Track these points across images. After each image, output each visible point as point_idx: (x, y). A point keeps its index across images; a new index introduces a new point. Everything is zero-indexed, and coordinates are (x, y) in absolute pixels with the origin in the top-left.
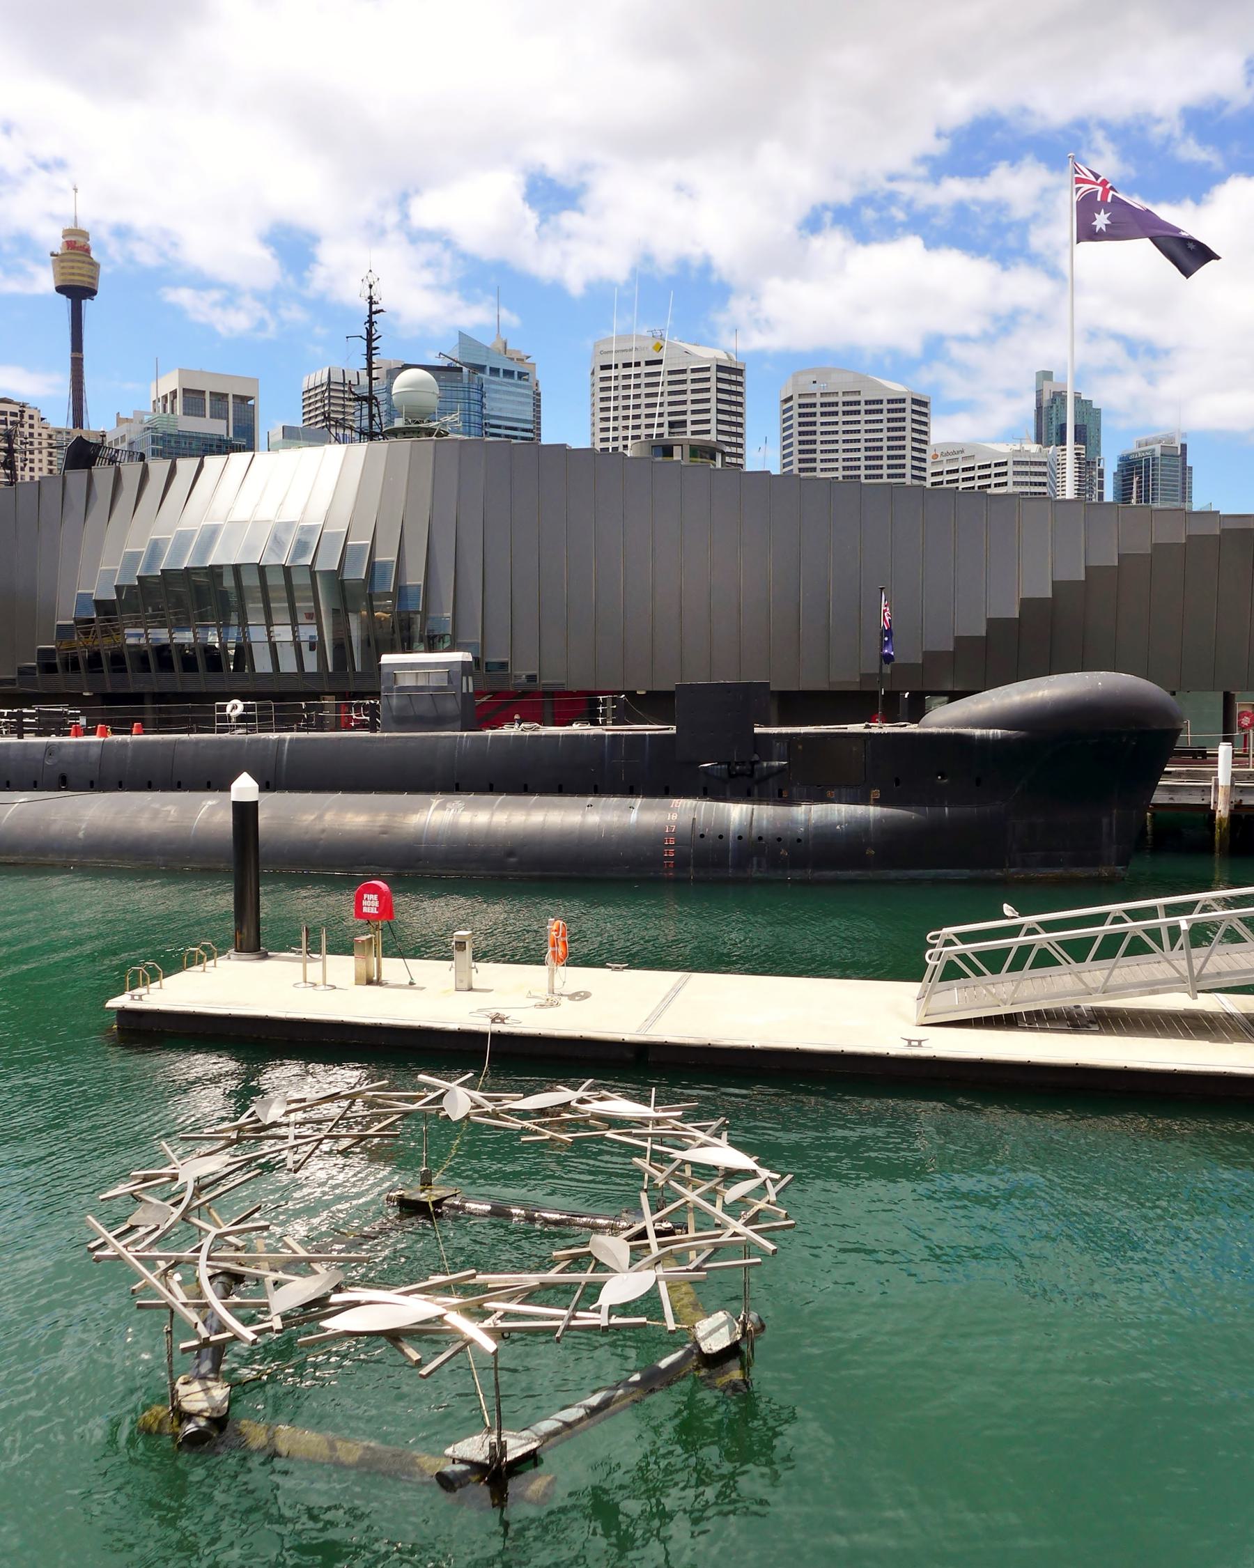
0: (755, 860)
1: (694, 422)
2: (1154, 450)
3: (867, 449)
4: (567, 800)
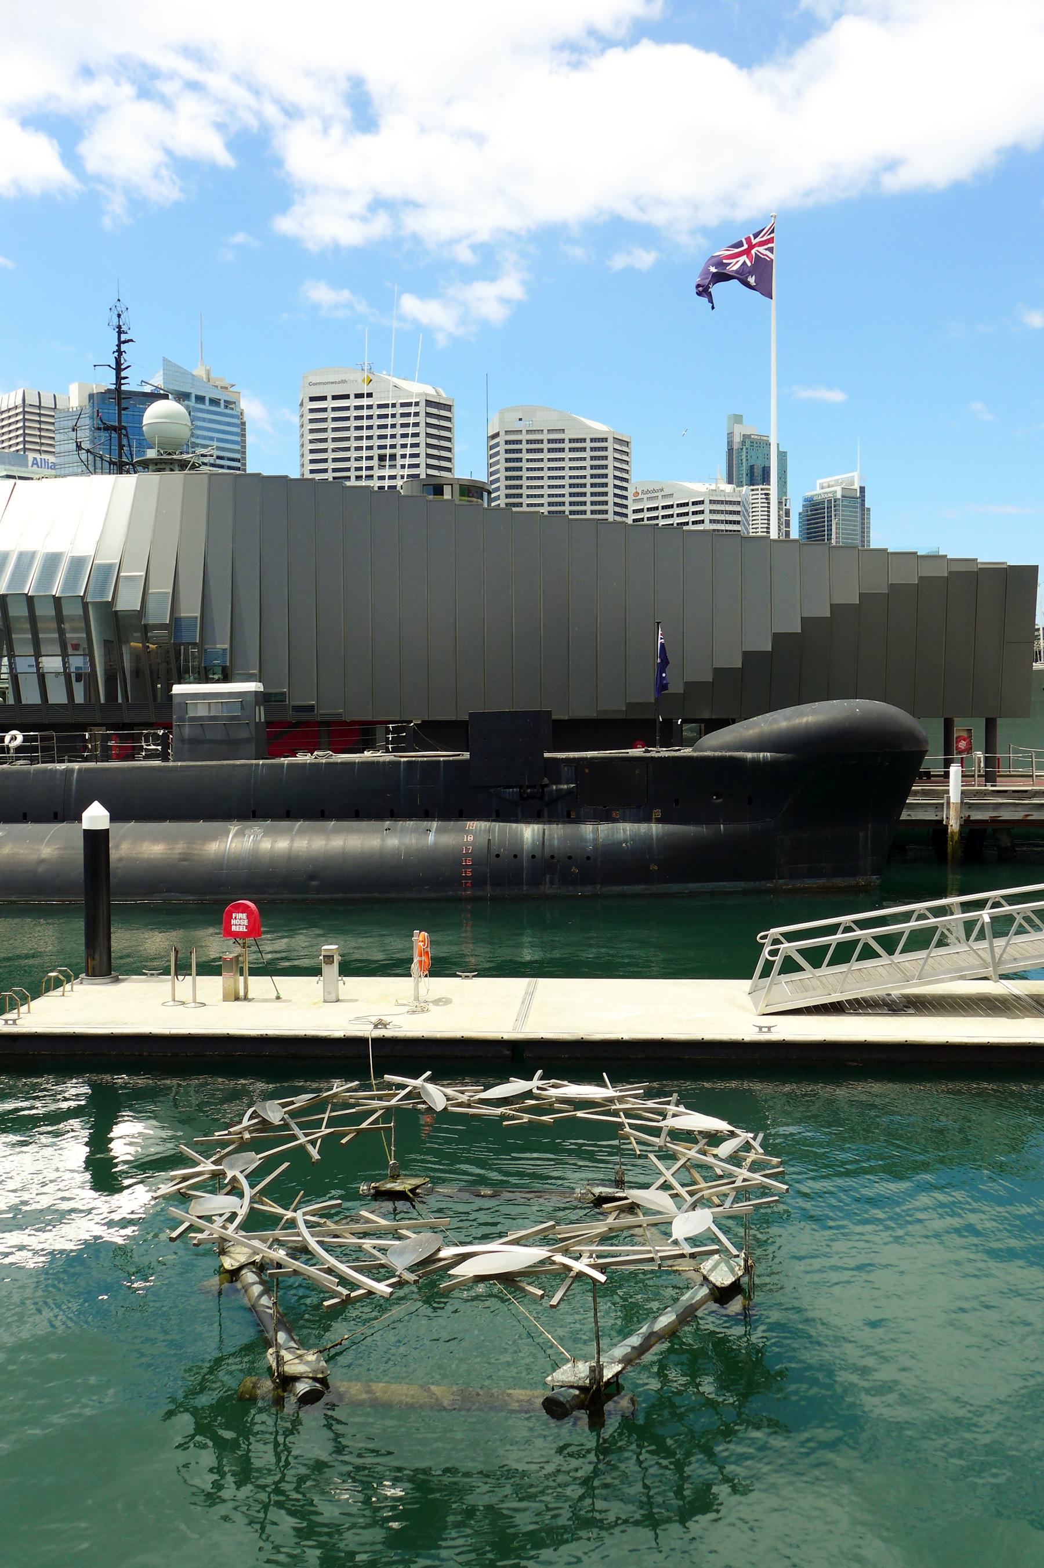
0: (548, 876)
2: (836, 492)
3: (571, 486)
4: (364, 824)
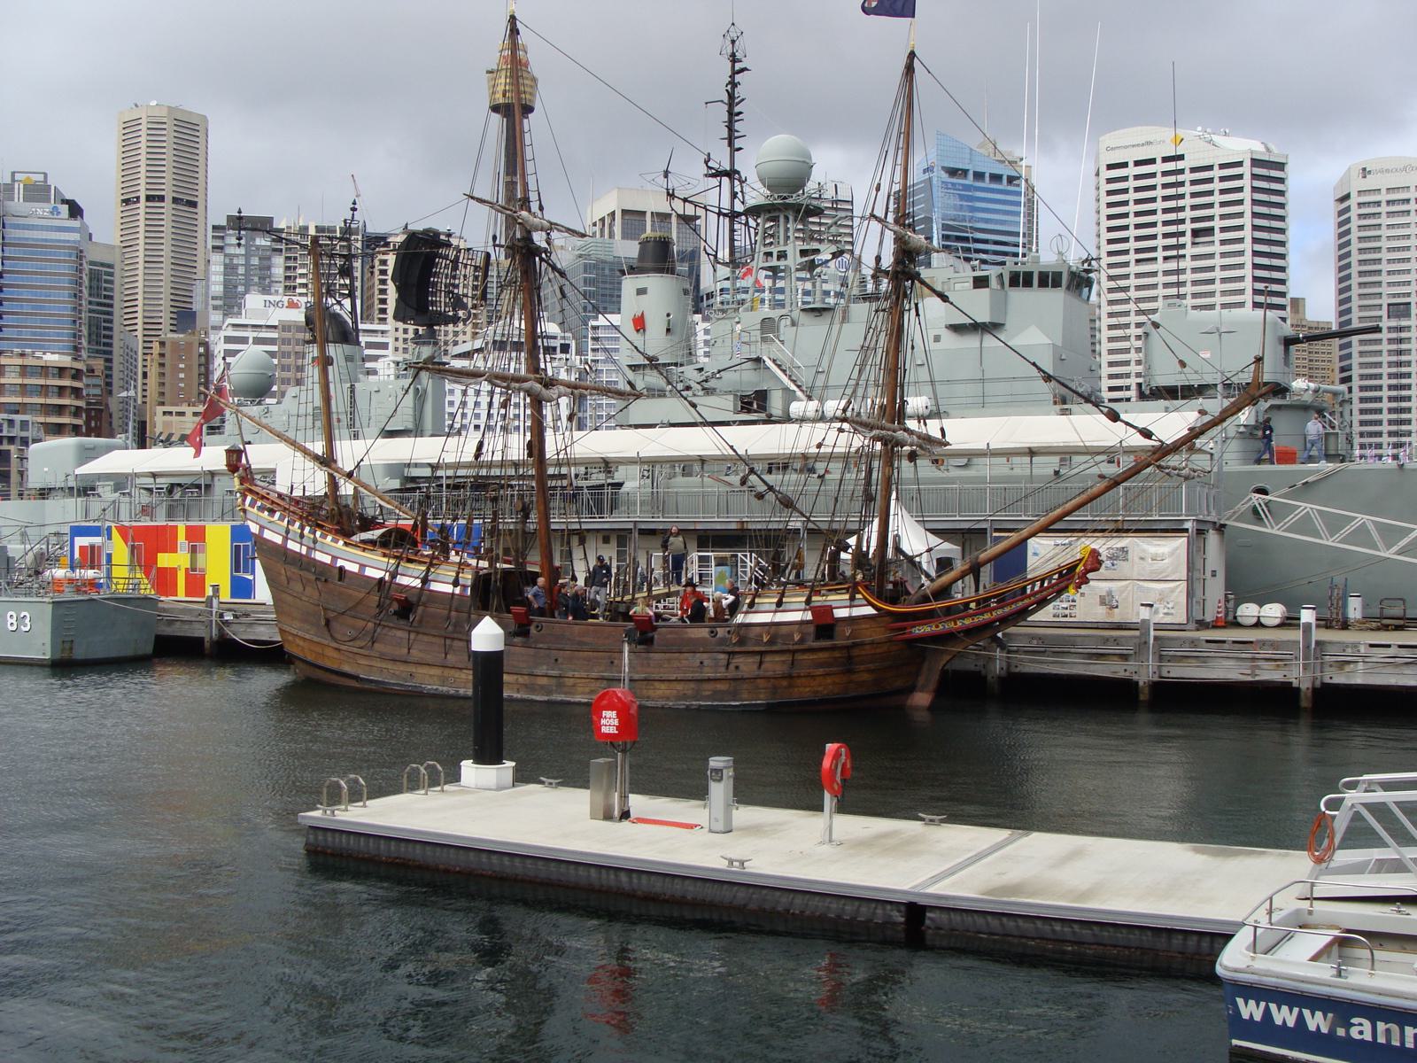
1: (1223, 230)
